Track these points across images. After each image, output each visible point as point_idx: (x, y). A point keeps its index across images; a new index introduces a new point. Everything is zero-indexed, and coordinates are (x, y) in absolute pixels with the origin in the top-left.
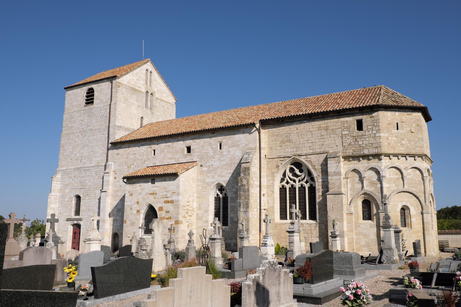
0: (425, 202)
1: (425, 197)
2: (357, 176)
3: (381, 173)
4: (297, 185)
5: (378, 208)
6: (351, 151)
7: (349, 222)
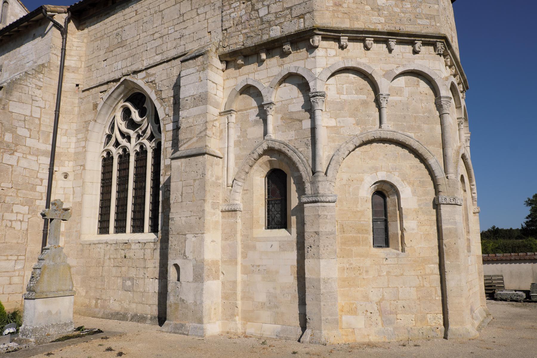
0: (446, 171)
1: (445, 156)
2: (254, 104)
3: (311, 84)
4: (133, 147)
5: (301, 191)
6: (241, 38)
7: (229, 235)
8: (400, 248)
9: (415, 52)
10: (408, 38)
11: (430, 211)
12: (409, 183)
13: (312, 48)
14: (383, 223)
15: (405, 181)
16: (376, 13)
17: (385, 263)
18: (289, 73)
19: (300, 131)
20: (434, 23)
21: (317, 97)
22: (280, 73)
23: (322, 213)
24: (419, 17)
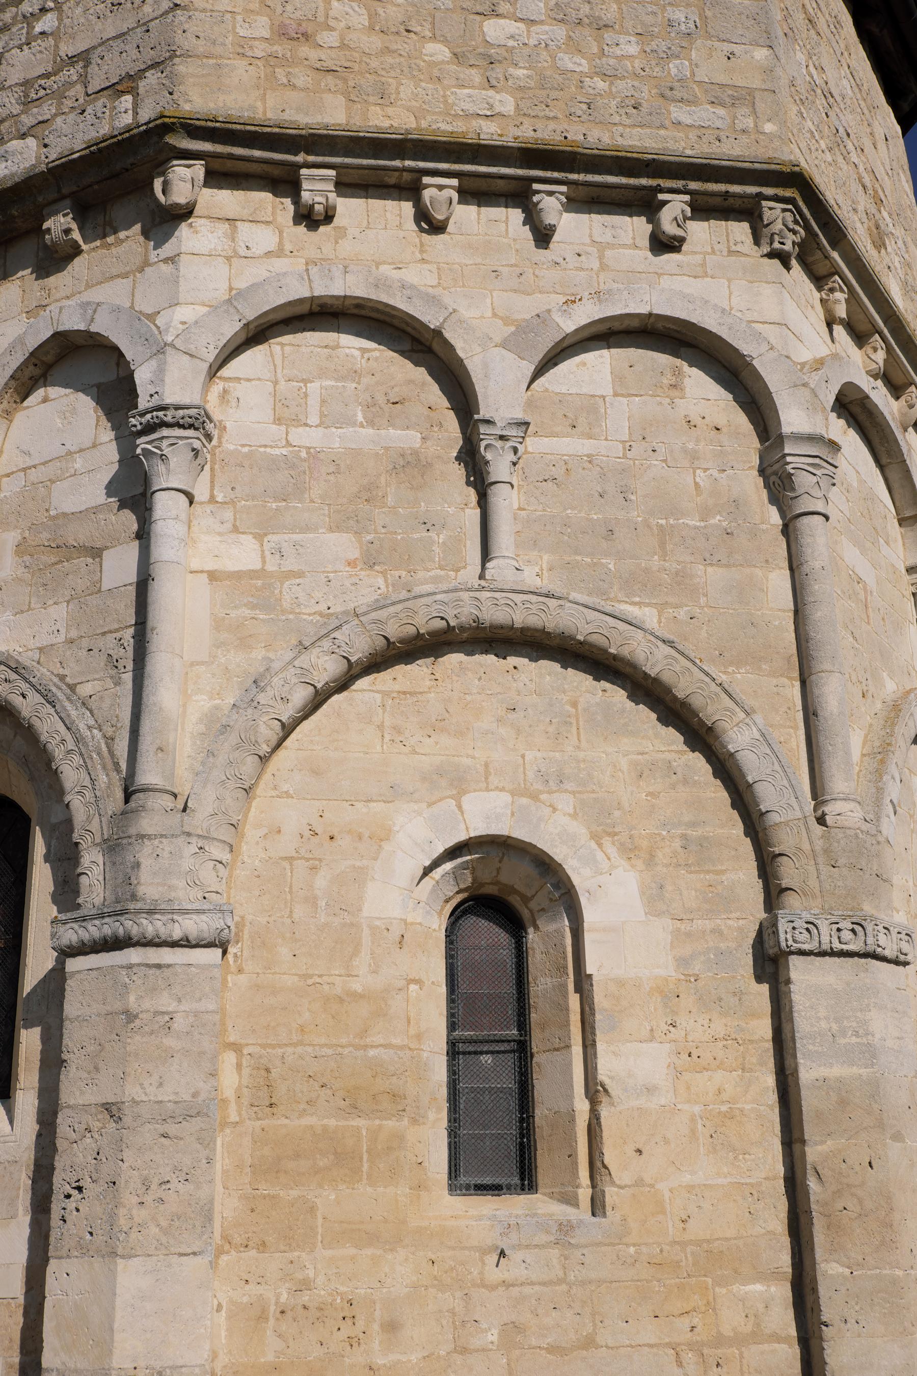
3: (142, 376)
8: (585, 1193)
9: (663, 244)
10: (624, 180)
11: (739, 994)
12: (629, 851)
13: (167, 220)
14: (510, 1061)
15: (607, 842)
16: (476, 76)
17: (494, 1274)
18: (57, 335)
19: (94, 601)
20: (750, 122)
21: (165, 432)
22: (20, 340)
23: (147, 1004)
24: (677, 94)
